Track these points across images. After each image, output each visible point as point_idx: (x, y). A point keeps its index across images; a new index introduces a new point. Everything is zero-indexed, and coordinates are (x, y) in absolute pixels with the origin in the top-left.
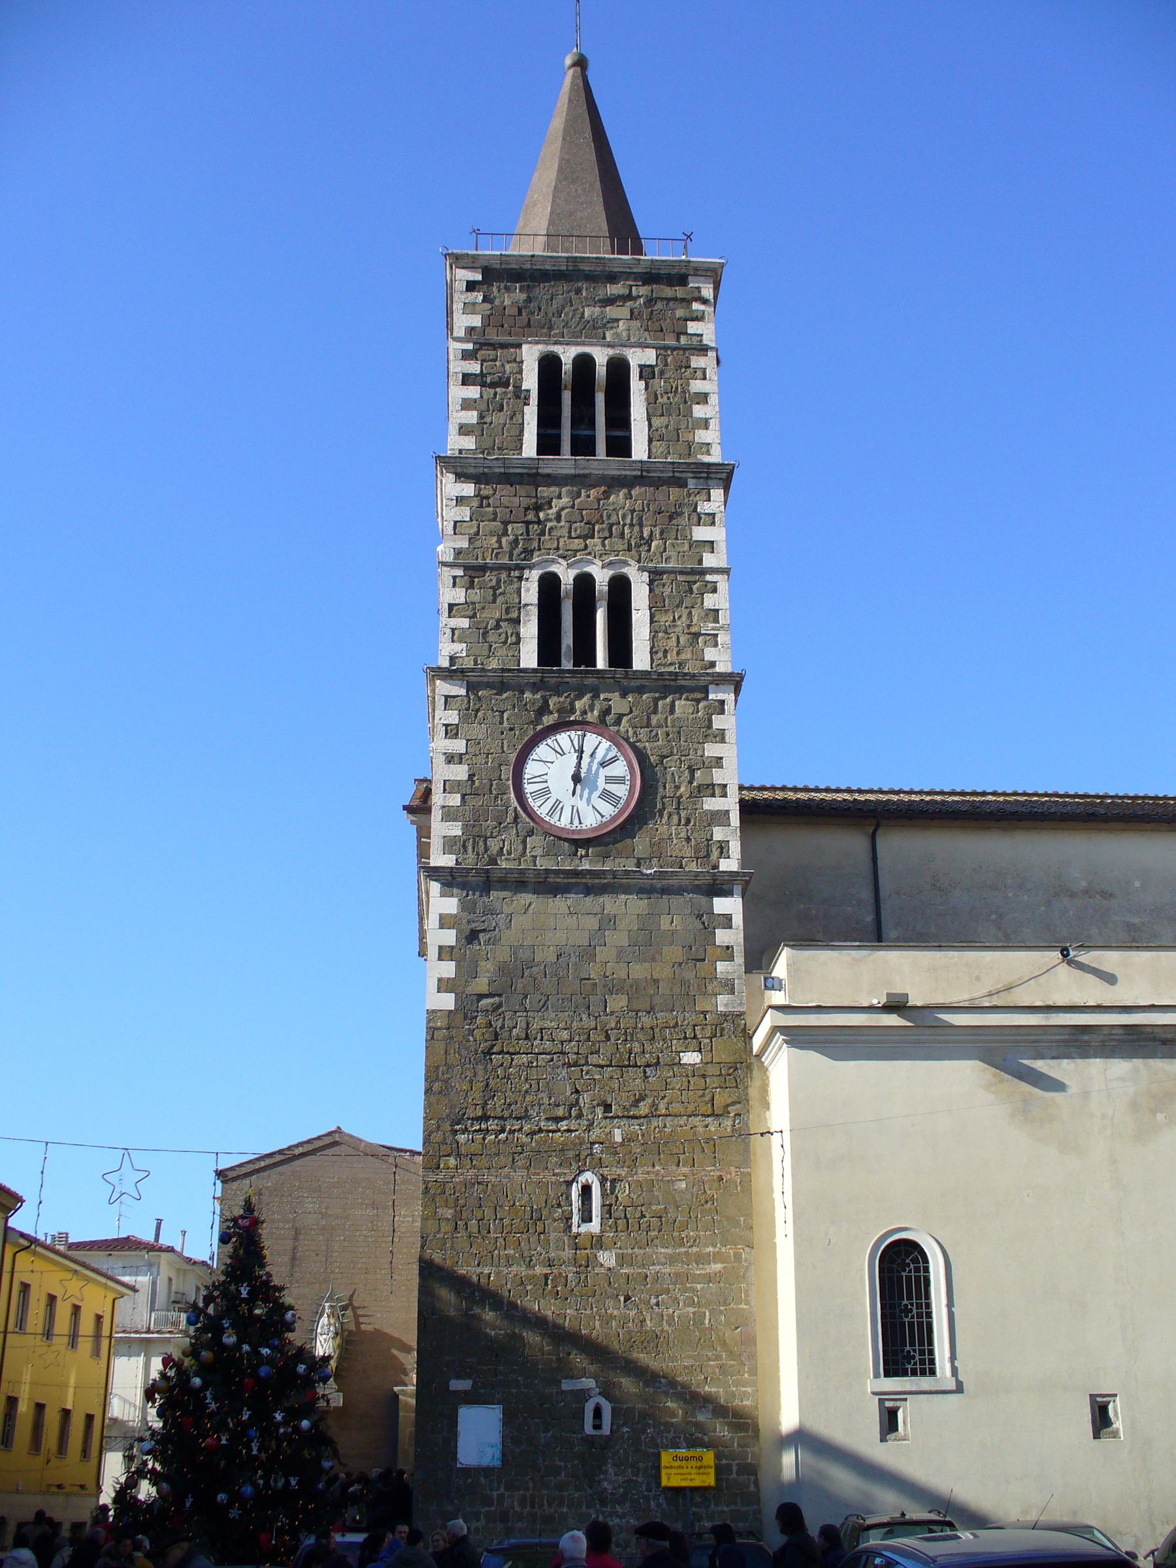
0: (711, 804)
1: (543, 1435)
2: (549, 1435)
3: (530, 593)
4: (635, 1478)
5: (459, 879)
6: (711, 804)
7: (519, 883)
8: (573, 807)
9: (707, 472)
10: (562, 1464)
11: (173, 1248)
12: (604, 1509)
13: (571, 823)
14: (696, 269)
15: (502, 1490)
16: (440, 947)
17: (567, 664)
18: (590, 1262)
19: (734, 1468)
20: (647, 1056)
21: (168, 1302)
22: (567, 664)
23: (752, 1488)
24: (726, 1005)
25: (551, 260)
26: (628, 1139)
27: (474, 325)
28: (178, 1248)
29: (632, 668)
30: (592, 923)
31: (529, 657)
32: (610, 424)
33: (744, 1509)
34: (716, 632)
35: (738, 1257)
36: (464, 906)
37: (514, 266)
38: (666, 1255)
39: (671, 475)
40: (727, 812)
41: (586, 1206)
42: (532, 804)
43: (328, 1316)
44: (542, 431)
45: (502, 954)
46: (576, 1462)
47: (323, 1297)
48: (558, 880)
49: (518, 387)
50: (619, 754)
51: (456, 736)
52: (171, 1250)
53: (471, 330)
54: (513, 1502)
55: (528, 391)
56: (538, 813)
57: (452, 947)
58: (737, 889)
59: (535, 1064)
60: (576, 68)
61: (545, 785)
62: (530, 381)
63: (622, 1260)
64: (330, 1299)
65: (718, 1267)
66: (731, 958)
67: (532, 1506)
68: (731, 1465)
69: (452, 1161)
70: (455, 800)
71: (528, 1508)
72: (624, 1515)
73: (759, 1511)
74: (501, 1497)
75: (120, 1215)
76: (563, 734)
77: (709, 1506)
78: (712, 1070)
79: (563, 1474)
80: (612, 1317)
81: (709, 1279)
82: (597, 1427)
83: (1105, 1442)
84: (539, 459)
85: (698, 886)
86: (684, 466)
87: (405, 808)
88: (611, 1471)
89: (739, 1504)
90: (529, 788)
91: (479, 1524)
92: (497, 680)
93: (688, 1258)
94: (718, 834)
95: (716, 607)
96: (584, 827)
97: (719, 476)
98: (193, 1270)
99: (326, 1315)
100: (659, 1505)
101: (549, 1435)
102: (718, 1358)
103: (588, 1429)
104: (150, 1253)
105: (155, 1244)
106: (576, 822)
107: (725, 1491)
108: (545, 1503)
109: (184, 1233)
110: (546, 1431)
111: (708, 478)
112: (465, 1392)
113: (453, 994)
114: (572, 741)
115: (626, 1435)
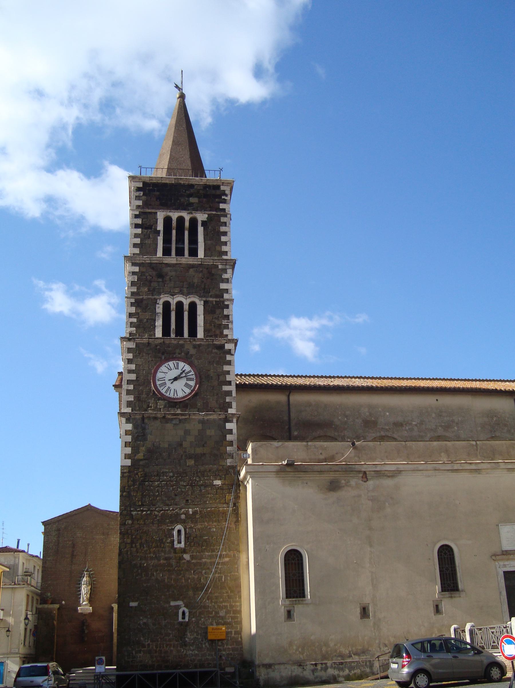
0: (226, 388)
1: (164, 622)
2: (166, 621)
3: (159, 309)
4: (197, 637)
5: (133, 417)
6: (226, 388)
8: (174, 389)
9: (226, 263)
10: (171, 632)
11: (24, 551)
12: (186, 648)
13: (174, 395)
14: (223, 183)
15: (149, 642)
16: (126, 442)
17: (173, 335)
18: (182, 558)
19: (233, 633)
20: (201, 482)
21: (23, 572)
22: (173, 335)
23: (240, 639)
24: (230, 463)
25: (168, 179)
26: (195, 513)
27: (139, 205)
28: (26, 551)
29: (197, 337)
30: (181, 433)
32: (190, 243)
33: (237, 647)
34: (228, 324)
35: (234, 556)
37: (155, 181)
38: (208, 556)
39: (212, 263)
40: (231, 391)
41: (179, 538)
42: (159, 389)
43: (86, 577)
44: (165, 245)
46: (176, 631)
47: (84, 571)
48: (169, 417)
49: (156, 229)
50: (192, 370)
51: (131, 363)
52: (23, 551)
54: (153, 646)
55: (160, 231)
56: (162, 392)
57: (130, 442)
58: (235, 420)
59: (160, 485)
60: (181, 99)
61: (164, 381)
62: (160, 227)
63: (192, 557)
64: (87, 571)
65: (227, 559)
66: (232, 445)
67: (160, 647)
68: (232, 632)
70: (131, 387)
71: (159, 648)
72: (193, 650)
73: (242, 647)
74: (149, 645)
75: (3, 538)
76: (171, 362)
77: (224, 646)
78: (225, 487)
79: (171, 636)
80: (189, 578)
82: (184, 618)
83: (290, 623)
84: (163, 257)
85: (220, 418)
86: (217, 260)
87: (113, 386)
88: (188, 634)
89: (235, 645)
90: (158, 383)
91: (141, 655)
92: (146, 342)
94: (228, 399)
95: (229, 314)
96: (179, 397)
97: (230, 264)
98: (33, 559)
99: (85, 577)
100: (206, 646)
101: (166, 621)
102: (227, 592)
103: (180, 619)
104: (15, 553)
105: (17, 549)
106: (176, 395)
107: (230, 641)
108: (165, 646)
109: (28, 545)
110: (165, 620)
111: (226, 265)
112: (135, 607)
113: (130, 460)
114: (174, 365)
115: (194, 621)
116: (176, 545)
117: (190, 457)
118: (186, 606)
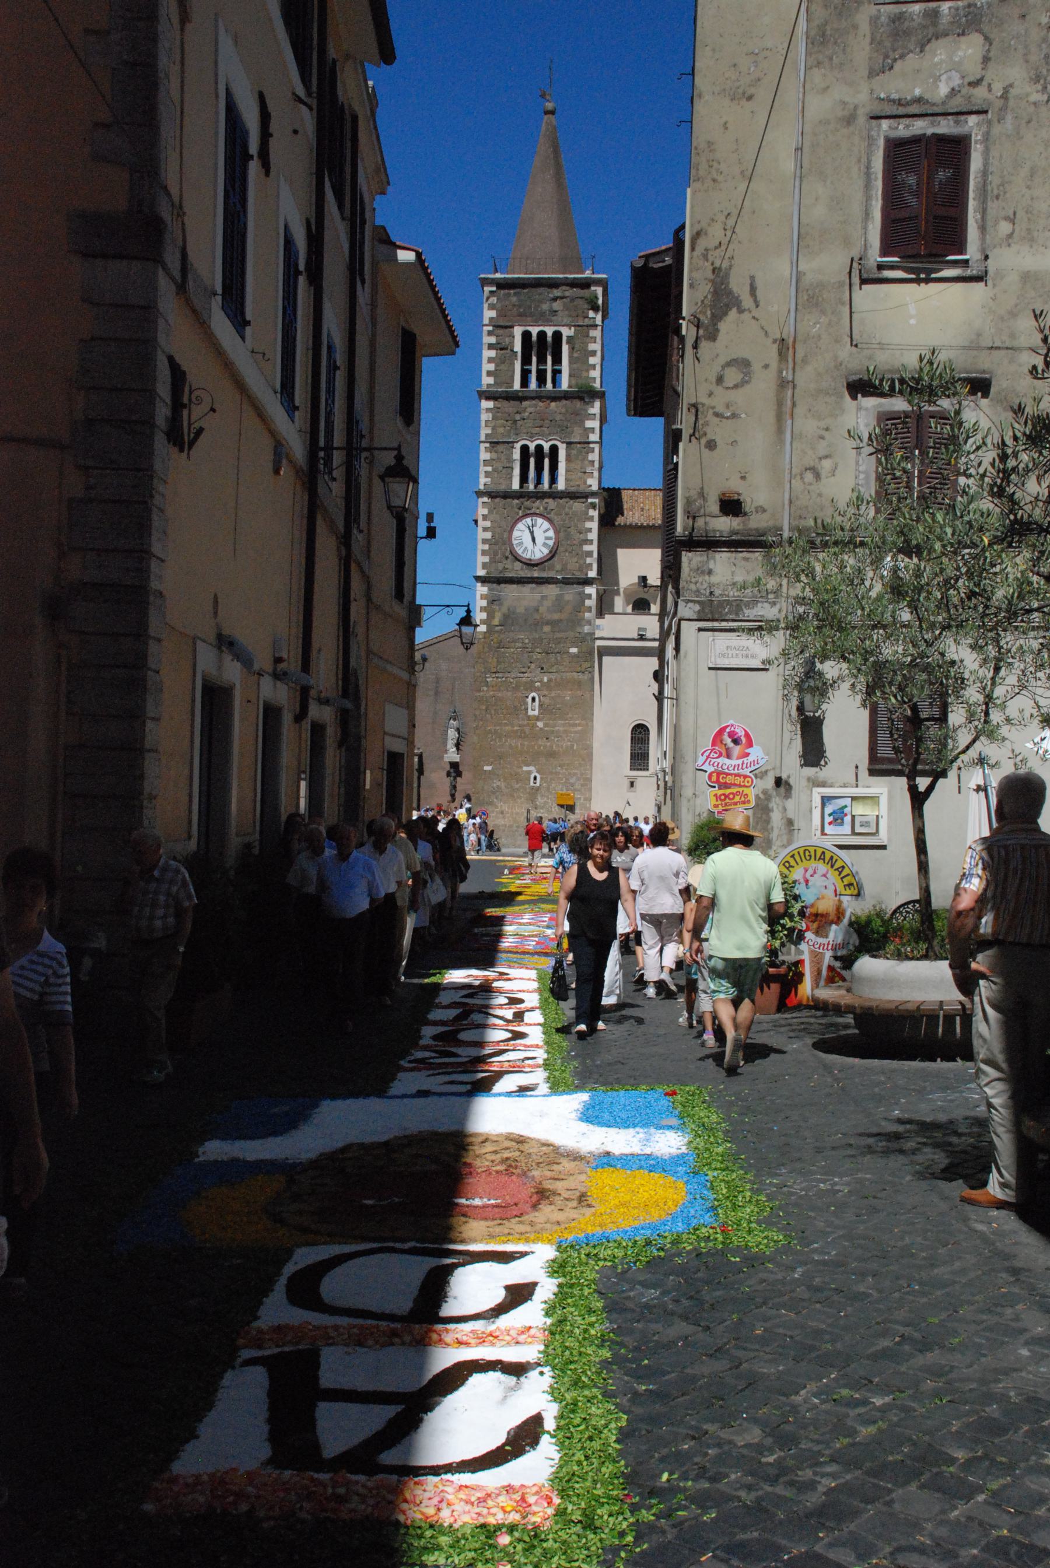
3: (517, 455)
6: (587, 548)
7: (511, 581)
26: (550, 680)
31: (516, 485)
36: (490, 590)
45: (504, 609)
49: (512, 350)
53: (491, 319)
62: (518, 347)
63: (546, 725)
69: (485, 689)
81: (576, 732)
93: (570, 725)
94: (588, 560)
103: (532, 784)
116: (530, 713)
117: (547, 623)
118: (538, 772)
